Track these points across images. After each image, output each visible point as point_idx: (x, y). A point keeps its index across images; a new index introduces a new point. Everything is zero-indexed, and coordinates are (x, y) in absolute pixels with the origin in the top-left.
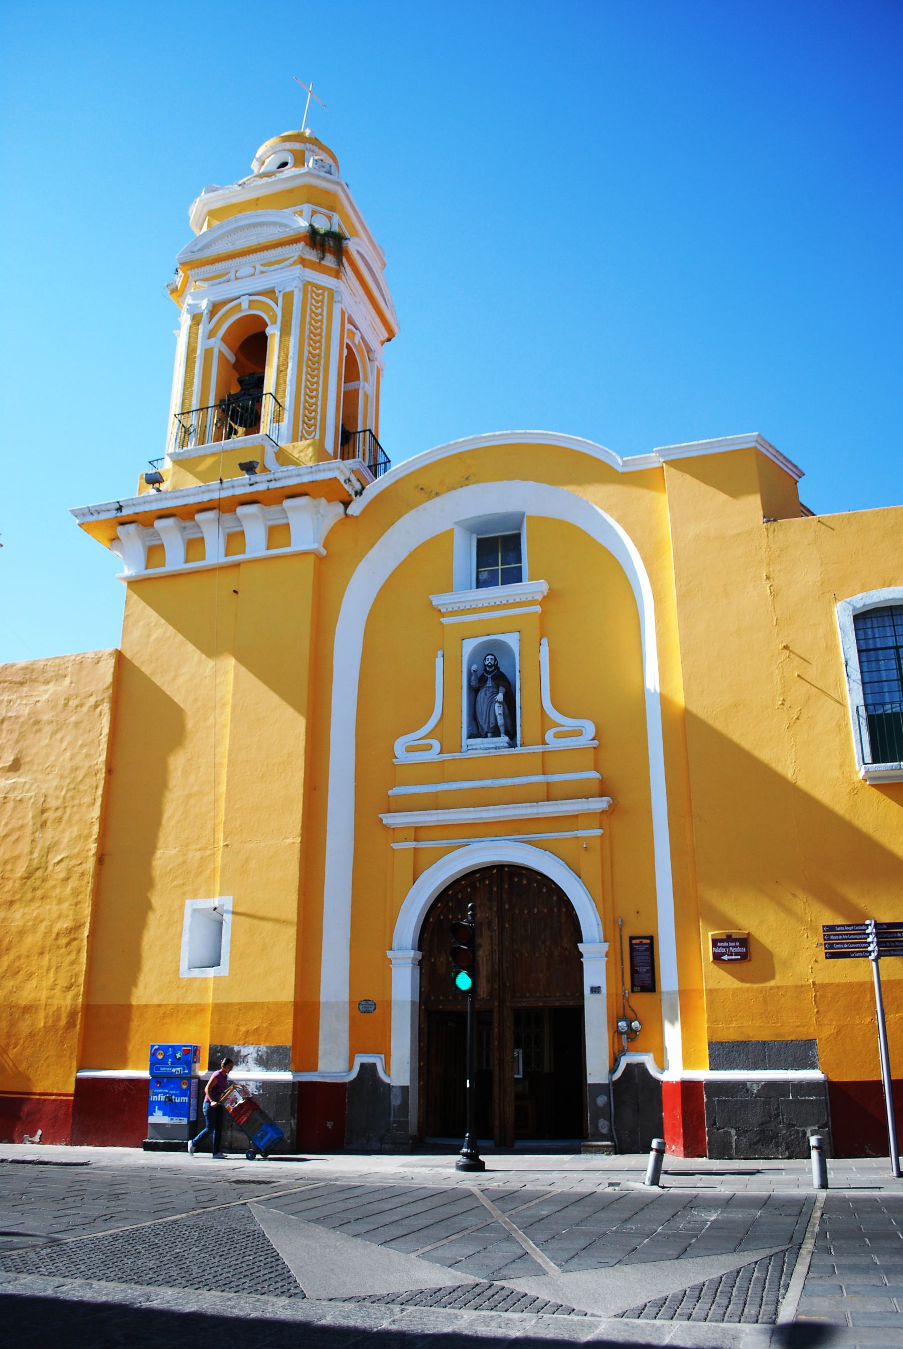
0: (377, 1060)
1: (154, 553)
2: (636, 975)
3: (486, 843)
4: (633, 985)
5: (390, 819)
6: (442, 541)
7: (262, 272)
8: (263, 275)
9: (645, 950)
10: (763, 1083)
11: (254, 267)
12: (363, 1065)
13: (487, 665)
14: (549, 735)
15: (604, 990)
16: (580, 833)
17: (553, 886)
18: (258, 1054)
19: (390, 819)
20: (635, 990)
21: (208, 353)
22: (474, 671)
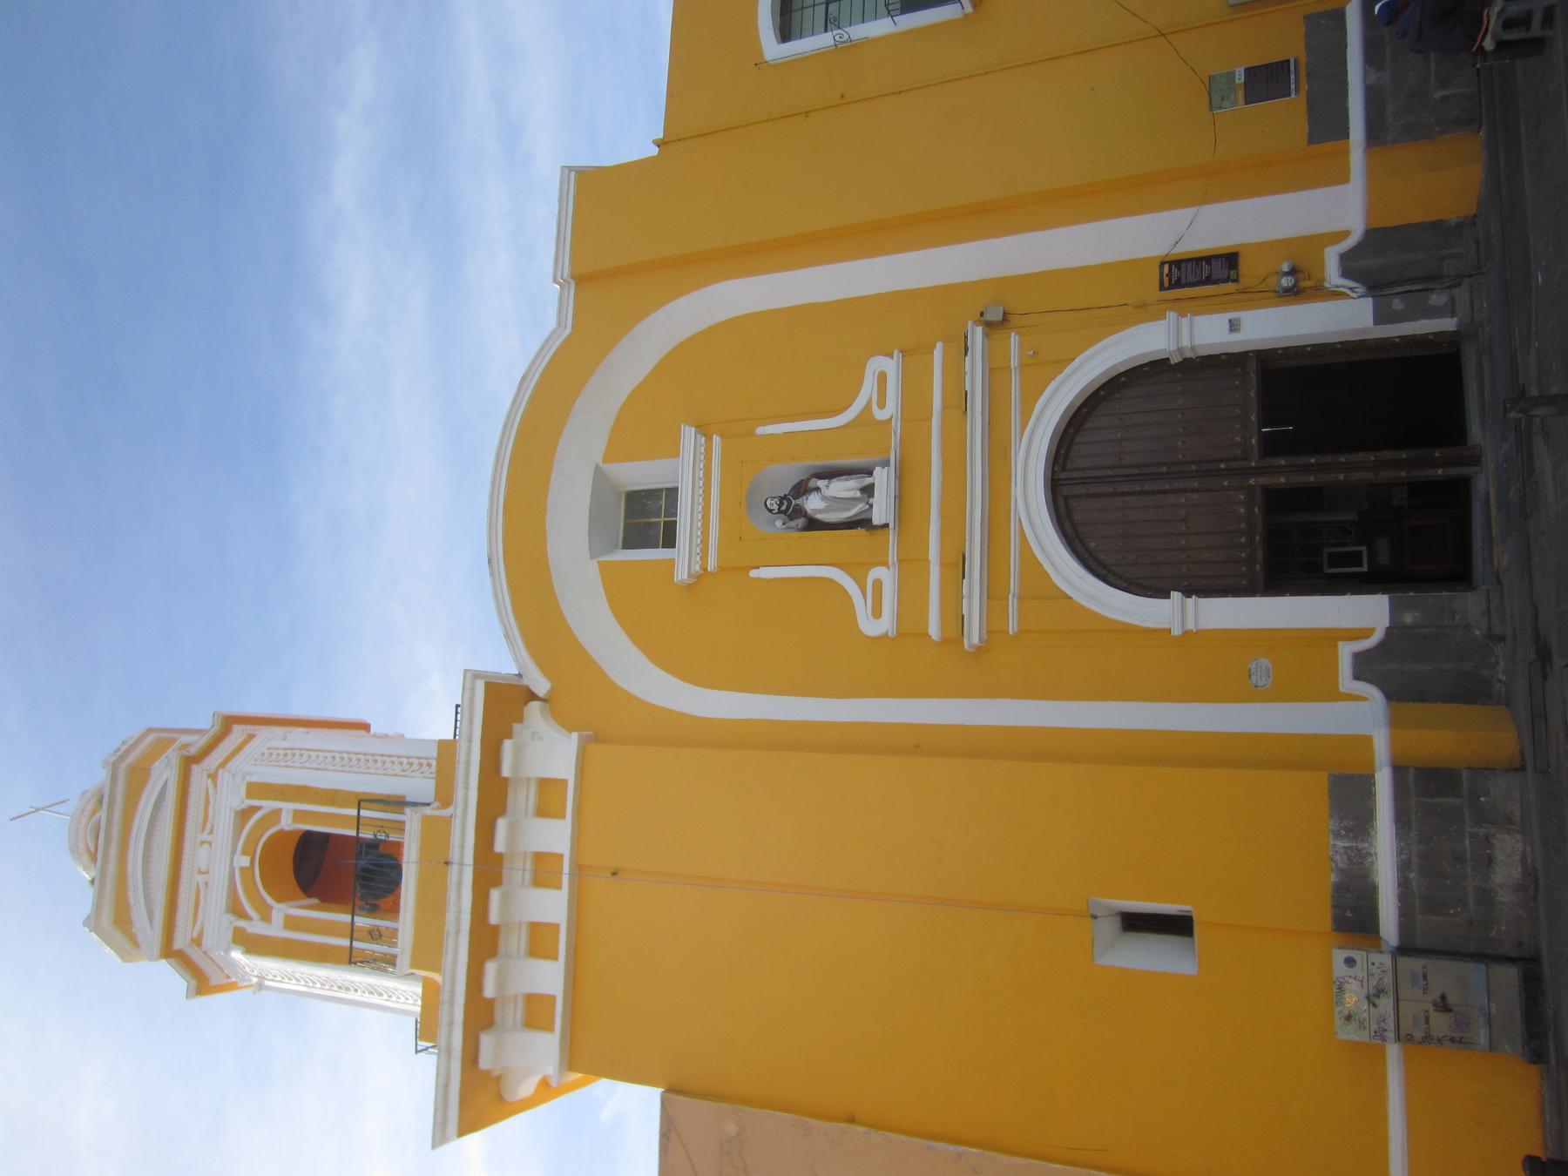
0: (1346, 652)
1: (536, 1012)
2: (1214, 277)
3: (1017, 491)
4: (1227, 280)
5: (974, 636)
7: (211, 832)
8: (215, 831)
9: (1179, 269)
10: (1367, 67)
11: (203, 843)
12: (1357, 676)
13: (779, 509)
14: (881, 415)
15: (1235, 337)
16: (1014, 363)
18: (1346, 836)
19: (974, 636)
21: (291, 923)
22: (784, 524)
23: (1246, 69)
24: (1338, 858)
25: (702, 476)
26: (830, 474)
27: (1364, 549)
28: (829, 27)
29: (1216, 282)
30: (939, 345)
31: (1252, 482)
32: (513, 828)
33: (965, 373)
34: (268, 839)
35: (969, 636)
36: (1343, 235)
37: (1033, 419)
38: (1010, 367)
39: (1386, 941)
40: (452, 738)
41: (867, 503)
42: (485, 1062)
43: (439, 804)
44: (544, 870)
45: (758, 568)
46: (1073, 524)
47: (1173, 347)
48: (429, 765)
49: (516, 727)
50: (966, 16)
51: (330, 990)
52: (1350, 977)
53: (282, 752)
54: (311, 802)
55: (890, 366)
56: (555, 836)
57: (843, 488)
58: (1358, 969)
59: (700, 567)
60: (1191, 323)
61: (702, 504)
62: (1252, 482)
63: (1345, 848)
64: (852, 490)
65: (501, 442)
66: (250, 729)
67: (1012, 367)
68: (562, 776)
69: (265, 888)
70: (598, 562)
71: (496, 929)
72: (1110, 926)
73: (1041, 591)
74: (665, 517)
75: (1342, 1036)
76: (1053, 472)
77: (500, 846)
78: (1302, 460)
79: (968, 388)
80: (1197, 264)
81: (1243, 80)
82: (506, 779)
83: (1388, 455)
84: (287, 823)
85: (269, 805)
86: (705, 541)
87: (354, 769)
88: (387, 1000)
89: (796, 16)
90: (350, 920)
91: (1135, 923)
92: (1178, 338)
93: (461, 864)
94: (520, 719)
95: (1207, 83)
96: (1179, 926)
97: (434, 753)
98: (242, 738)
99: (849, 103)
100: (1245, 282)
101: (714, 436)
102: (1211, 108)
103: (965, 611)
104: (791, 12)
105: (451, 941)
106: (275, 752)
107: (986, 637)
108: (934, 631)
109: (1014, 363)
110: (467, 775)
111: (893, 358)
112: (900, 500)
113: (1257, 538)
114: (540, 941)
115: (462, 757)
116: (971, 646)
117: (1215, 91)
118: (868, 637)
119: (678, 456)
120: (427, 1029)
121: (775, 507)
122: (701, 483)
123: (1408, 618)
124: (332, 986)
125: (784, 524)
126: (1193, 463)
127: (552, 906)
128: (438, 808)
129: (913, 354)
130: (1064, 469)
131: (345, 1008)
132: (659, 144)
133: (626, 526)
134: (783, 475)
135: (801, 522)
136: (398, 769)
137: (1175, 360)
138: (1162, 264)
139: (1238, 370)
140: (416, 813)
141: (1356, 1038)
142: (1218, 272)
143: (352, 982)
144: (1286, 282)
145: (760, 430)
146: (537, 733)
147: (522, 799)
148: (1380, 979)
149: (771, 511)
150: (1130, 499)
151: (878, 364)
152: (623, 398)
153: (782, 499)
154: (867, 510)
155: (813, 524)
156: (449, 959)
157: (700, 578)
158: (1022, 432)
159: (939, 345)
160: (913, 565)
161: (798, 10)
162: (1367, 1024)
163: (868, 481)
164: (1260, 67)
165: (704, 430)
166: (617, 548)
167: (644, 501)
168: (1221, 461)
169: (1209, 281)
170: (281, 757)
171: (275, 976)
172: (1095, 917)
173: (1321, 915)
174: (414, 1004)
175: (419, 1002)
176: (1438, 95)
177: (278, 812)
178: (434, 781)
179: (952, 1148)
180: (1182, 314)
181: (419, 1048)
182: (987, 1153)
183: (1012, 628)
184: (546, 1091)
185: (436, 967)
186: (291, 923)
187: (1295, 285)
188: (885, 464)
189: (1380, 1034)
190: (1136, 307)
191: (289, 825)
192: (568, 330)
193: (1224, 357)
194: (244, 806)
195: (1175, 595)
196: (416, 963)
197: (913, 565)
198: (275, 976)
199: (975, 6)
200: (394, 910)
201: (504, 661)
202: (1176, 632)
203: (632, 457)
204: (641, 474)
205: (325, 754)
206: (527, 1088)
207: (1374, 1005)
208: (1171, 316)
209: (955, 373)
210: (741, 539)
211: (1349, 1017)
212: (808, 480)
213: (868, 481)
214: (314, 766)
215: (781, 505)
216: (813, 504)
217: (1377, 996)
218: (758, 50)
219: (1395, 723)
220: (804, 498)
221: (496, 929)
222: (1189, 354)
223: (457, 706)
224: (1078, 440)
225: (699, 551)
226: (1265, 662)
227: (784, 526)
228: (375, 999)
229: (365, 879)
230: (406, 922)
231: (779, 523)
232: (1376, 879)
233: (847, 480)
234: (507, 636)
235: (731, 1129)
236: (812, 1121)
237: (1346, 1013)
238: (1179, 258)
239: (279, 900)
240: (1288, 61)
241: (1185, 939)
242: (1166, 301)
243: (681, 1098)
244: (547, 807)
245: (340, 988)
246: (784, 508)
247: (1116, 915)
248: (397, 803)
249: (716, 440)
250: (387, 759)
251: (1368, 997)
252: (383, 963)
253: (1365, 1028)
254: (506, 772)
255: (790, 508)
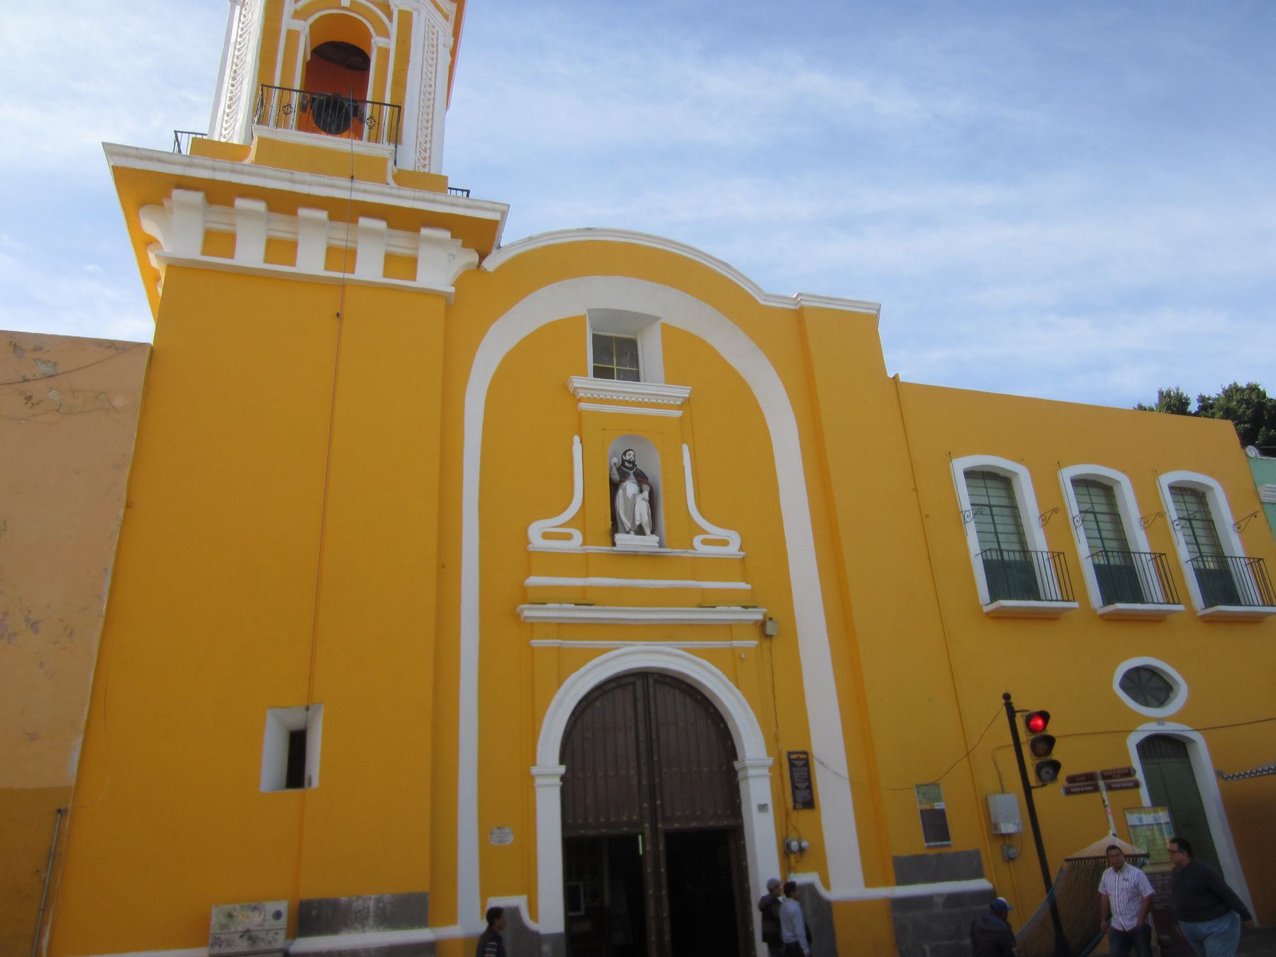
0: (518, 901)
1: (220, 241)
2: (797, 792)
3: (640, 646)
4: (795, 801)
5: (530, 612)
6: (573, 324)
14: (697, 541)
15: (755, 809)
16: (736, 643)
17: (699, 697)
19: (530, 612)
20: (797, 807)
21: (293, 36)
22: (615, 464)
23: (943, 810)
24: (360, 902)
25: (652, 401)
26: (653, 502)
27: (582, 912)
28: (978, 507)
29: (794, 794)
30: (748, 587)
31: (647, 825)
32: (377, 234)
33: (729, 606)
34: (366, 25)
35: (530, 609)
36: (827, 885)
37: (694, 657)
38: (732, 640)
39: (292, 943)
40: (449, 186)
41: (630, 530)
42: (178, 194)
43: (395, 172)
44: (342, 257)
45: (581, 442)
46: (613, 689)
47: (748, 763)
48: (424, 166)
49: (460, 242)
50: (981, 607)
51: (233, 62)
52: (265, 916)
53: (435, 43)
54: (395, 65)
55: (733, 549)
56: (369, 268)
57: (642, 510)
58: (271, 922)
59: (581, 397)
60: (763, 776)
61: (598, 398)
62: (647, 825)
63: (368, 908)
64: (641, 519)
65: (680, 244)
66: (453, 17)
67: (733, 642)
68: (298, 263)
69: (322, 17)
70: (585, 315)
71: (294, 213)
72: (296, 721)
73: (566, 664)
74: (617, 369)
75: (215, 911)
76: (653, 674)
77: (364, 222)
78: (663, 863)
79: (718, 608)
80: (806, 779)
81: (936, 808)
82: (419, 231)
83: (667, 926)
84: (377, 42)
85: (393, 28)
86: (601, 401)
87: (422, 103)
88: (224, 112)
89: (980, 483)
90: (386, 103)
91: (297, 742)
92: (754, 767)
93: (351, 189)
94: (464, 245)
95: (937, 782)
96: (295, 775)
97: (433, 171)
98: (445, 10)
99: (922, 521)
100: (794, 815)
101: (681, 412)
102: (918, 786)
103: (549, 605)
104: (984, 479)
105: (285, 175)
106: (435, 37)
107: (528, 621)
108: (533, 580)
109: (736, 643)
110: (424, 200)
111: (739, 551)
112: (635, 555)
113: (604, 830)
114: (281, 249)
115: (439, 197)
116: (522, 610)
117: (929, 789)
118: (527, 527)
119: (666, 383)
120: (202, 146)
121: (628, 458)
122: (646, 400)
123: (546, 948)
124: (236, 65)
125: (615, 464)
126: (661, 780)
127: (311, 261)
128: (393, 171)
129: (741, 567)
130: (656, 681)
131: (216, 75)
132: (896, 378)
133: (610, 338)
134: (651, 464)
135: (616, 477)
136: (421, 140)
137: (737, 765)
138: (805, 753)
139: (729, 812)
140: (390, 154)
141: (213, 923)
142: (802, 795)
143: (241, 83)
144: (794, 845)
145: (685, 448)
146: (454, 258)
147: (401, 243)
148: (263, 940)
149: (624, 454)
150: (632, 733)
151: (735, 539)
152: (710, 341)
153: (633, 463)
154: (625, 529)
155: (614, 487)
156: (270, 172)
157: (574, 397)
158: (683, 649)
159: (748, 587)
160: (584, 564)
161: (985, 484)
162: (226, 931)
163: (648, 531)
164: (945, 820)
165: (686, 404)
166: (594, 329)
167: (629, 354)
168: (662, 801)
169: (795, 788)
170: (431, 41)
171: (245, 16)
172: (307, 709)
173: (313, 890)
174: (221, 134)
175: (223, 140)
176: (927, 948)
177: (387, 36)
178: (413, 170)
179: (106, 590)
180: (771, 769)
181: (179, 134)
182: (102, 619)
183: (536, 642)
184: (144, 244)
185: (259, 160)
186: (293, 36)
187: (792, 852)
188: (661, 545)
189: (218, 942)
190: (776, 734)
191: (376, 43)
192: (762, 302)
193: (738, 801)
194: (392, 7)
195: (562, 769)
196: (262, 141)
197: (584, 564)
198: (245, 16)
199: (988, 614)
200: (302, 126)
201: (511, 236)
202: (534, 770)
203: (665, 346)
204: (651, 352)
205: (433, 78)
206: (150, 227)
207: (242, 936)
208: (770, 761)
209: (728, 598)
210: (604, 429)
211: (230, 916)
212: (648, 484)
213: (648, 531)
214: (424, 70)
215: (629, 462)
216: (630, 487)
217: (250, 938)
218: (960, 455)
219: (466, 940)
220: (635, 481)
221: (294, 213)
222: (740, 775)
223: (468, 192)
224: (677, 692)
225: (594, 396)
226: (511, 839)
227: (613, 464)
228: (224, 101)
229: (335, 102)
230: (293, 136)
231: (615, 460)
232: (344, 933)
233: (648, 514)
234: (530, 239)
235: (119, 402)
236: (127, 472)
237: (235, 914)
238: (811, 765)
239: (312, 27)
240: (949, 840)
241: (284, 786)
242: (780, 756)
243: (146, 360)
244: (392, 262)
245: (235, 72)
246: (627, 464)
247: (305, 727)
248: (396, 137)
249: (679, 413)
250: (429, 132)
251: (248, 931)
252: (260, 112)
253: (222, 929)
254: (425, 232)
255: (626, 470)
